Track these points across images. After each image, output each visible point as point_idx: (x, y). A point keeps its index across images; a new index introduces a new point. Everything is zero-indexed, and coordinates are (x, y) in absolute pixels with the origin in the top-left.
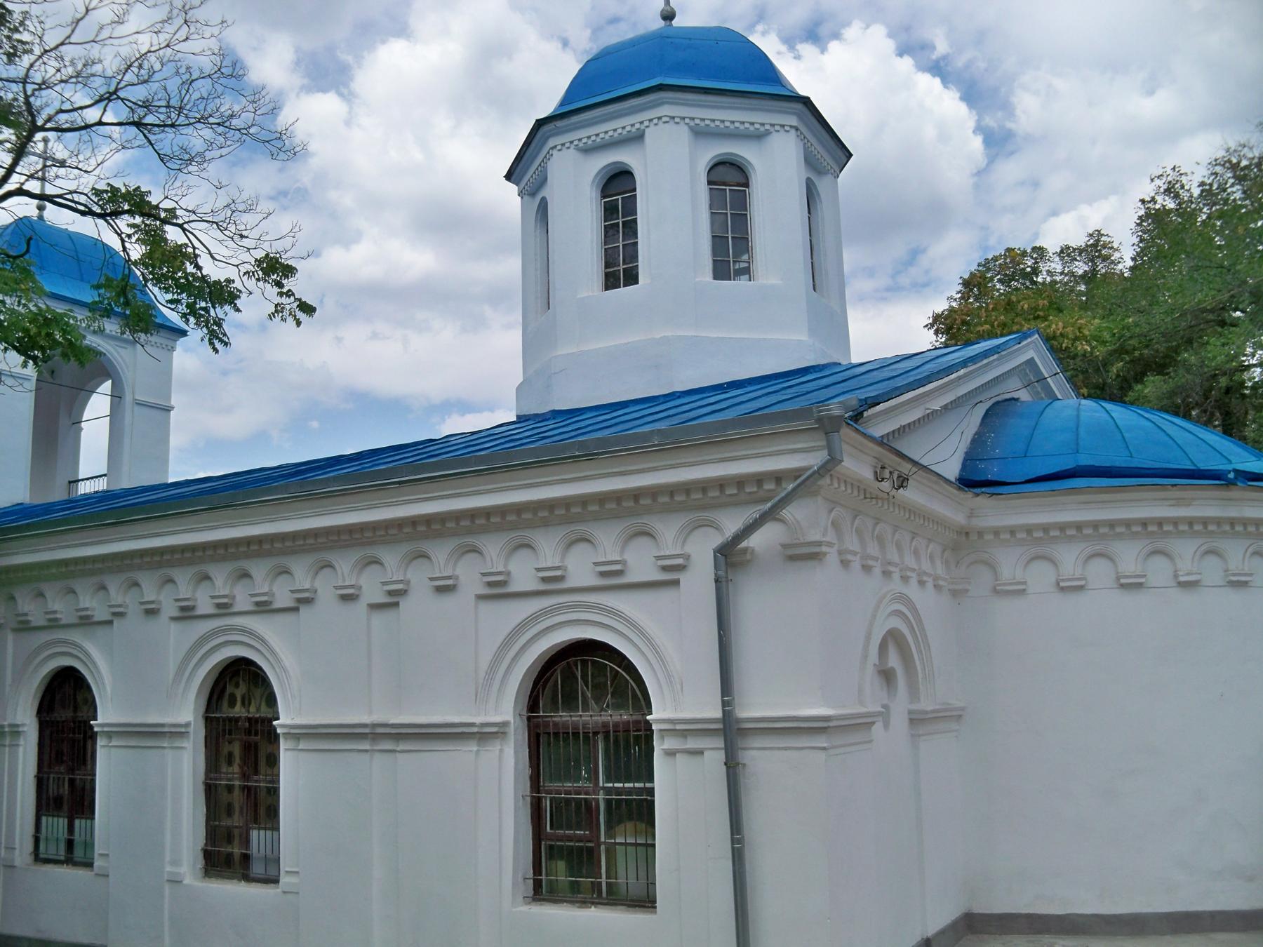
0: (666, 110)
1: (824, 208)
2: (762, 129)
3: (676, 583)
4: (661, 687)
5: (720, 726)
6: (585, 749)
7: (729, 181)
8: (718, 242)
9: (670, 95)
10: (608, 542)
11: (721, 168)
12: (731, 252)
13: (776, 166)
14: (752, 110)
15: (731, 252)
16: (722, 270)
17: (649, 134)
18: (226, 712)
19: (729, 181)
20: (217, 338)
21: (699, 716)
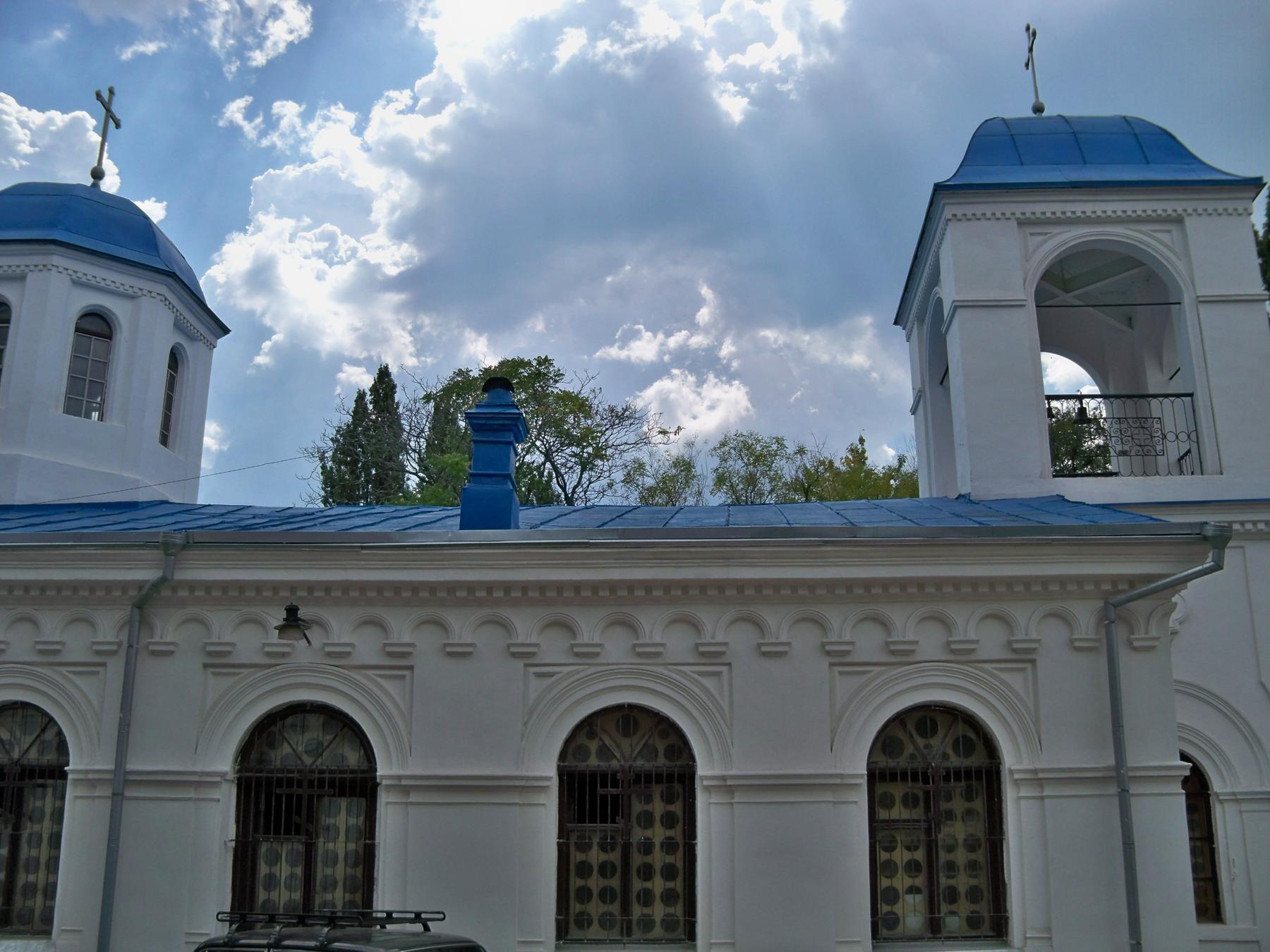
0: (56, 260)
1: (188, 374)
2: (18, 271)
3: (104, 665)
4: (1019, 751)
5: (1113, 774)
6: (937, 782)
7: (96, 327)
8: (75, 380)
9: (60, 249)
10: (52, 626)
11: (89, 319)
12: (86, 390)
13: (146, 327)
14: (30, 254)
15: (86, 390)
16: (75, 406)
17: (30, 277)
18: (55, 730)
19: (96, 327)
20: (566, 495)
21: (767, 772)
